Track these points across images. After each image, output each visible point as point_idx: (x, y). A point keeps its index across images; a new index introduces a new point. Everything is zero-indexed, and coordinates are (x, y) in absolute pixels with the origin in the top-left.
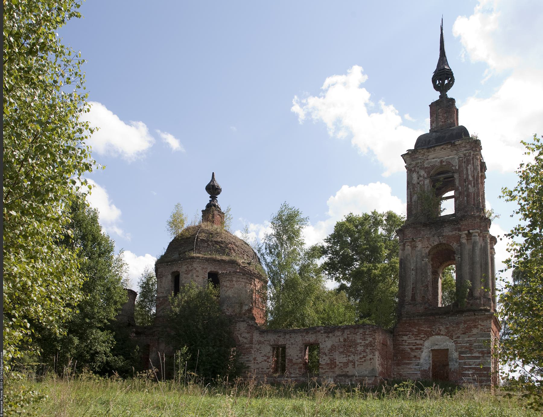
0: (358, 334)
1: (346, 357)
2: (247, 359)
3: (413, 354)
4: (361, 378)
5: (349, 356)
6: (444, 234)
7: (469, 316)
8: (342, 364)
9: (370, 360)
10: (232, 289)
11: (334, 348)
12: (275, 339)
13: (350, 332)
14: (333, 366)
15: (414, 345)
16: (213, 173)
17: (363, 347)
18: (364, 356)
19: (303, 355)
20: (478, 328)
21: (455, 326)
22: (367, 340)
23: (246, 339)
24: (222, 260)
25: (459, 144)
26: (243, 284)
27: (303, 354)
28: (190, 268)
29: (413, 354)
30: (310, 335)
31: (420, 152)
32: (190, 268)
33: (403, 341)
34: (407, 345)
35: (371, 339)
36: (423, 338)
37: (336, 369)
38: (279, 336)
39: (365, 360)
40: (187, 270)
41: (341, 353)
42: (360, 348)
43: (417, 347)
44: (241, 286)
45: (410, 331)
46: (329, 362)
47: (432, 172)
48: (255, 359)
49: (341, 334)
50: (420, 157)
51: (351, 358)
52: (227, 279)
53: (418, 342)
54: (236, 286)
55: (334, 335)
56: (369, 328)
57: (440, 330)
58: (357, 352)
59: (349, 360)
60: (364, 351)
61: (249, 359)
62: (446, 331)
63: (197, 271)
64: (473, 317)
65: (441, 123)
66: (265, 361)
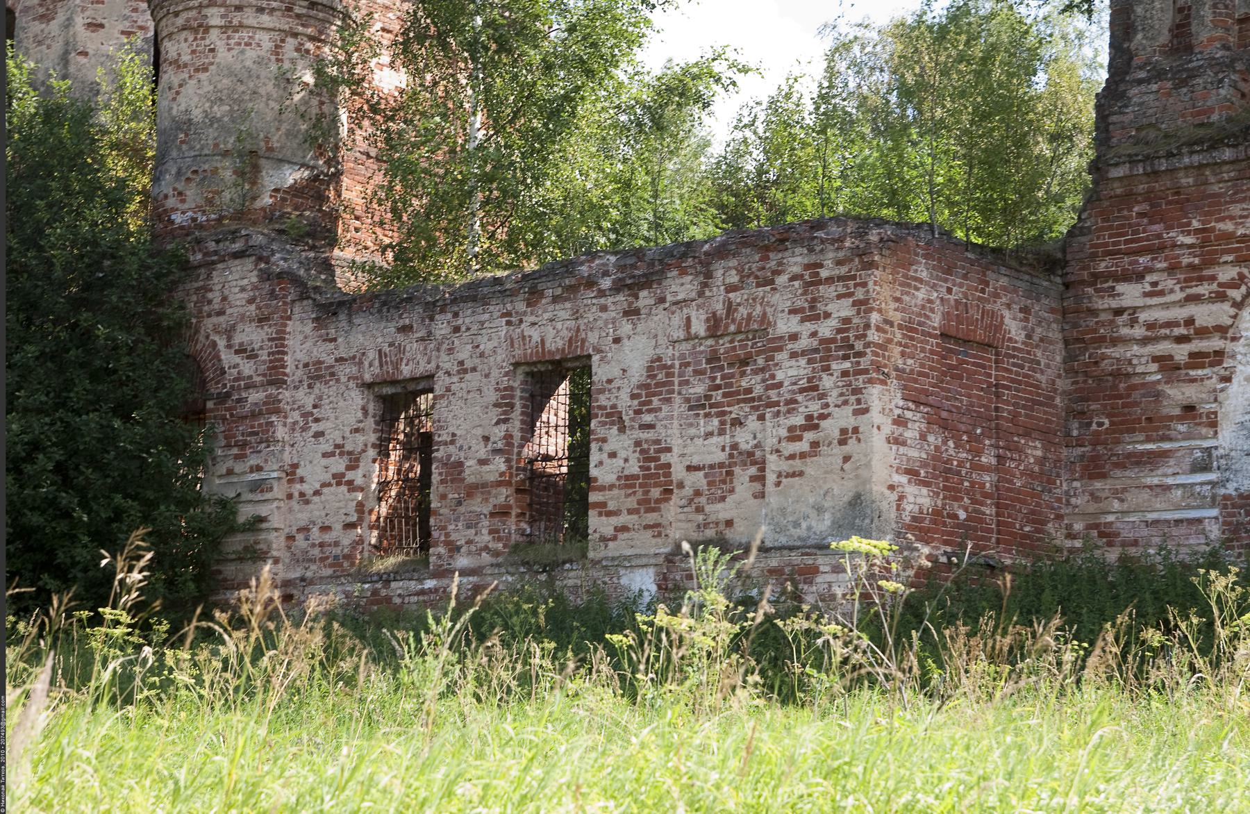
0: (782, 280)
1: (722, 432)
2: (255, 476)
3: (1178, 394)
4: (795, 558)
5: (737, 422)
8: (699, 479)
9: (842, 442)
10: (203, 76)
11: (661, 376)
12: (386, 349)
13: (740, 271)
14: (655, 493)
15: (1181, 340)
17: (803, 362)
18: (809, 418)
19: (517, 435)
22: (827, 315)
23: (252, 356)
27: (516, 426)
29: (1178, 394)
30: (546, 310)
33: (1119, 312)
34: (1144, 341)
35: (842, 309)
36: (1234, 285)
37: (671, 510)
38: (407, 329)
39: (815, 444)
41: (696, 405)
42: (790, 371)
43: (1197, 345)
44: (251, 54)
45: (1155, 250)
46: (634, 468)
48: (291, 474)
49: (696, 286)
51: (744, 439)
52: (180, 21)
53: (1205, 314)
54: (223, 56)
55: (662, 300)
56: (841, 240)
58: (773, 394)
59: (734, 446)
60: (812, 388)
61: (263, 475)
66: (339, 478)
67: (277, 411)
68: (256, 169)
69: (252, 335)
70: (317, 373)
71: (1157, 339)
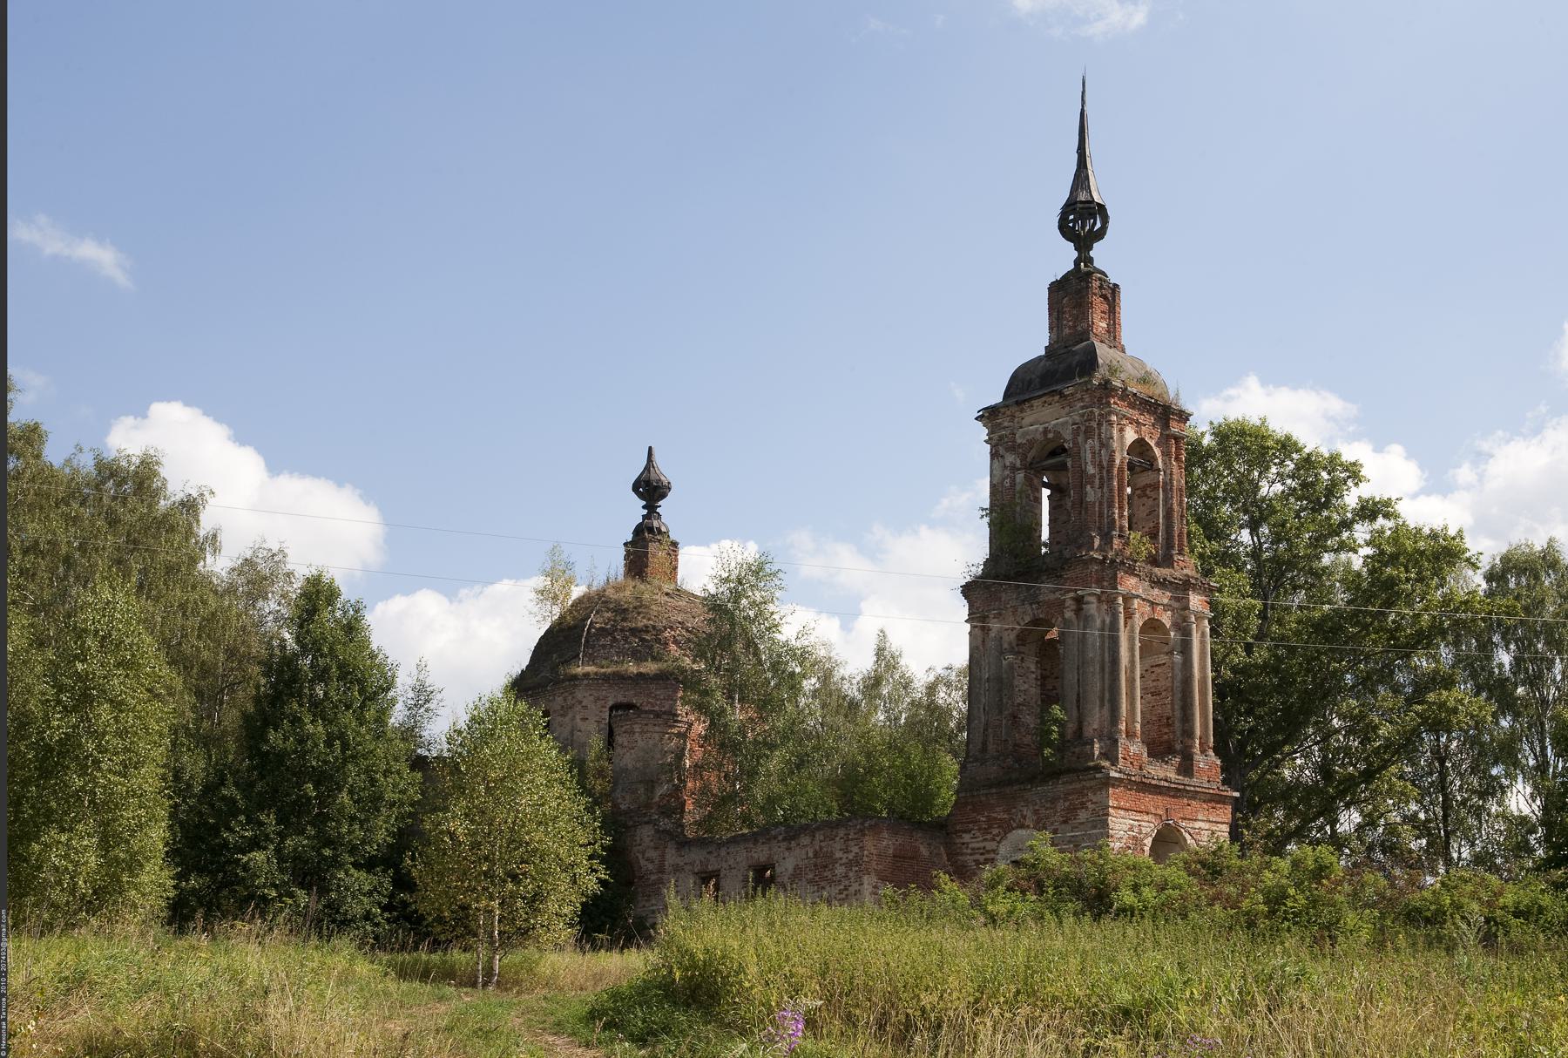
0: (837, 839)
5: (823, 888)
6: (1041, 598)
7: (1071, 783)
15: (982, 854)
16: (650, 448)
20: (1087, 808)
21: (1048, 805)
24: (640, 675)
25: (1072, 395)
26: (657, 738)
28: (570, 702)
31: (1004, 414)
32: (570, 702)
33: (963, 844)
34: (971, 854)
35: (855, 850)
38: (710, 853)
40: (563, 707)
41: (810, 882)
42: (840, 870)
43: (987, 856)
47: (1030, 456)
50: (1006, 424)
52: (623, 729)
53: (990, 845)
57: (1024, 817)
62: (1035, 818)
63: (585, 707)
64: (1077, 786)
65: (1067, 331)
67: (662, 883)
68: (653, 787)
69: (652, 854)
70: (677, 869)
71: (975, 854)
